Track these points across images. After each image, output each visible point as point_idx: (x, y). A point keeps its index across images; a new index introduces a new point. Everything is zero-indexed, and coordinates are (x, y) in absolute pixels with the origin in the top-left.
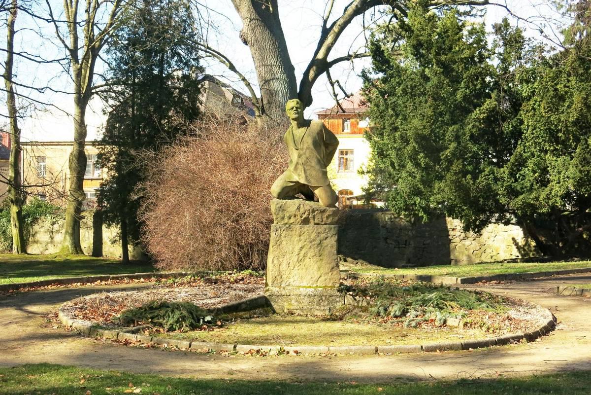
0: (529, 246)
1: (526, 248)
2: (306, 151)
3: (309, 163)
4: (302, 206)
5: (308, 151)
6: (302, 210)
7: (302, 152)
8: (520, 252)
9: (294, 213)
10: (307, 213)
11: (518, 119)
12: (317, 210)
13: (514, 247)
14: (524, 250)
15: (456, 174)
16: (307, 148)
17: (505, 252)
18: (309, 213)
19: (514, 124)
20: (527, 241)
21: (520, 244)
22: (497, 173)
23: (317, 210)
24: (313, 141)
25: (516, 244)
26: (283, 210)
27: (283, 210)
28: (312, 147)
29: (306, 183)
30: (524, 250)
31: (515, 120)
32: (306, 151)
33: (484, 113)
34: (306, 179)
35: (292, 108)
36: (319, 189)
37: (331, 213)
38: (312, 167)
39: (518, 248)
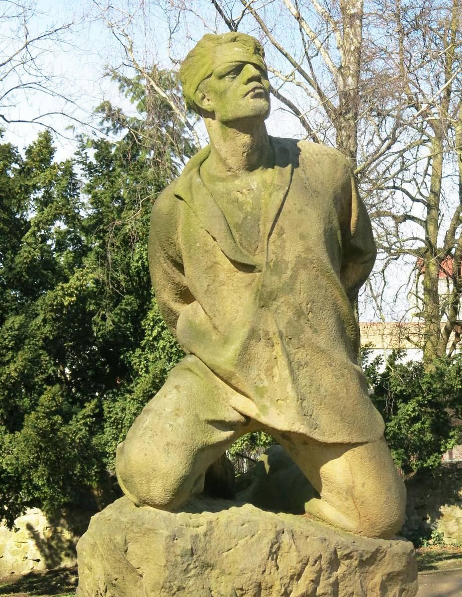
0: (60, 540)
1: (53, 543)
2: (293, 278)
3: (308, 333)
4: (286, 539)
5: (303, 276)
6: (289, 561)
7: (274, 282)
8: (42, 551)
9: (257, 577)
10: (309, 573)
11: (122, 310)
12: (348, 556)
13: (32, 543)
14: (50, 547)
15: (48, 415)
16: (302, 263)
17: (14, 553)
18: (319, 572)
19: (116, 320)
20: (55, 532)
21: (42, 537)
22: (109, 412)
23: (348, 556)
24: (325, 231)
25: (35, 536)
26: (206, 566)
27: (206, 566)
28: (321, 254)
29: (300, 428)
30: (50, 547)
31: (117, 310)
32: (293, 278)
33: (71, 295)
34: (305, 414)
35: (237, 69)
36: (348, 454)
37: (398, 567)
38: (320, 351)
39: (39, 544)
